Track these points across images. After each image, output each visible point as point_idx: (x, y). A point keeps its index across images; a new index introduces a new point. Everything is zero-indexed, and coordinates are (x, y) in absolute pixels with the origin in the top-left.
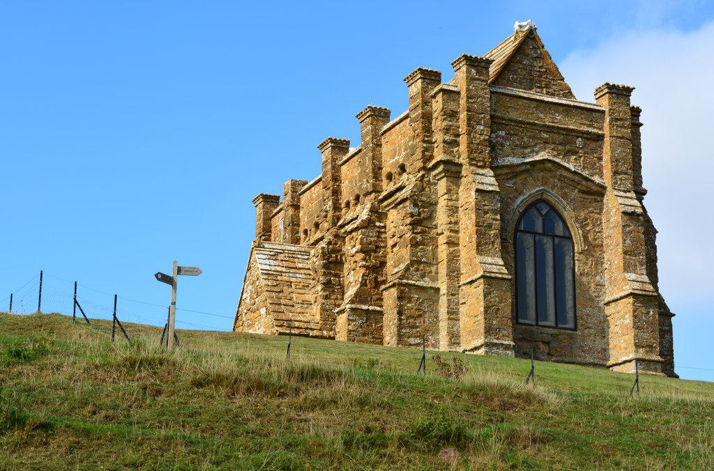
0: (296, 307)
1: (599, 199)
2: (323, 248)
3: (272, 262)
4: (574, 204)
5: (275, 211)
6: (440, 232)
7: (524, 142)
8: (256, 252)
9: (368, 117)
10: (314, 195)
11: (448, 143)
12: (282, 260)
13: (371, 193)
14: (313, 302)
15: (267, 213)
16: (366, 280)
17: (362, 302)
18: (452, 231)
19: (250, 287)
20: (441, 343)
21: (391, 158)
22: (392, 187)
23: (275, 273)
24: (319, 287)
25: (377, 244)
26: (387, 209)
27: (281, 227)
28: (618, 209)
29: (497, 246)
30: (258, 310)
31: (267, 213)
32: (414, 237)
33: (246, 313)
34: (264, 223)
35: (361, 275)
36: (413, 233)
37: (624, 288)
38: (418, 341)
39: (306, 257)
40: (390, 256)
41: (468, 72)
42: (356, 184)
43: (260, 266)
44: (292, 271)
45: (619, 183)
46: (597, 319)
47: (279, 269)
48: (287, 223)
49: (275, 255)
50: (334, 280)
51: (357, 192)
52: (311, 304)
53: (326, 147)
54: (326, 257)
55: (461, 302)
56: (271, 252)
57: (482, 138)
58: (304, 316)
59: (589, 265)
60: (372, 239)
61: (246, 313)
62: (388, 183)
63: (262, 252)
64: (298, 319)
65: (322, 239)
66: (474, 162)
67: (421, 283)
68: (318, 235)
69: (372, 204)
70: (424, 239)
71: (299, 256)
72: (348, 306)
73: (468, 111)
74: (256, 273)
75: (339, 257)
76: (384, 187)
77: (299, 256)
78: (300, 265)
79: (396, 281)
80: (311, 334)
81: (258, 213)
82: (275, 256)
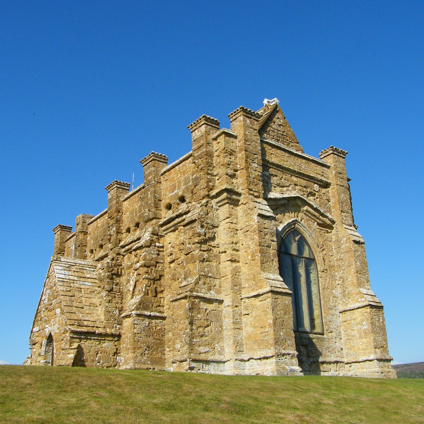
0: (85, 309)
1: (329, 231)
2: (108, 263)
3: (67, 273)
4: (315, 233)
5: (68, 237)
6: (222, 250)
7: (282, 182)
8: (54, 264)
9: (151, 161)
10: (99, 225)
11: (230, 176)
12: (74, 272)
13: (152, 220)
14: (98, 305)
15: (63, 238)
16: (148, 290)
17: (146, 308)
18: (234, 250)
19: (48, 291)
20: (226, 350)
21: (170, 192)
22: (170, 214)
23: (68, 281)
24: (104, 294)
25: (157, 261)
26: (166, 232)
27: (73, 248)
28: (349, 239)
29: (276, 264)
30: (54, 310)
31: (63, 238)
32: (202, 254)
33: (44, 311)
34: (61, 245)
35: (144, 285)
36: (201, 250)
37: (359, 300)
38: (207, 349)
39: (93, 269)
40: (167, 270)
41: (244, 121)
42: (136, 215)
43: (57, 275)
44: (82, 279)
45: (344, 219)
46: (336, 325)
47: (72, 278)
48: (78, 245)
49: (69, 267)
50: (116, 288)
51: (137, 220)
52: (97, 306)
53: (112, 188)
54: (110, 270)
55: (243, 313)
56: (66, 264)
57: (256, 174)
58: (92, 317)
59: (328, 280)
60: (154, 256)
61: (44, 311)
62: (167, 212)
63: (60, 265)
64: (87, 319)
65: (106, 256)
66: (251, 192)
67: (208, 296)
68: (102, 253)
69: (153, 228)
70: (209, 256)
71: (87, 269)
72: (134, 312)
73: (246, 151)
74: (54, 280)
75: (119, 270)
76: (163, 215)
77: (87, 269)
78: (88, 276)
79: (188, 294)
80: (97, 332)
81: (56, 238)
82: (69, 267)
